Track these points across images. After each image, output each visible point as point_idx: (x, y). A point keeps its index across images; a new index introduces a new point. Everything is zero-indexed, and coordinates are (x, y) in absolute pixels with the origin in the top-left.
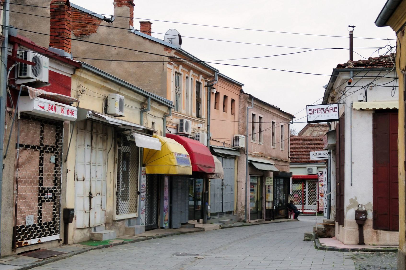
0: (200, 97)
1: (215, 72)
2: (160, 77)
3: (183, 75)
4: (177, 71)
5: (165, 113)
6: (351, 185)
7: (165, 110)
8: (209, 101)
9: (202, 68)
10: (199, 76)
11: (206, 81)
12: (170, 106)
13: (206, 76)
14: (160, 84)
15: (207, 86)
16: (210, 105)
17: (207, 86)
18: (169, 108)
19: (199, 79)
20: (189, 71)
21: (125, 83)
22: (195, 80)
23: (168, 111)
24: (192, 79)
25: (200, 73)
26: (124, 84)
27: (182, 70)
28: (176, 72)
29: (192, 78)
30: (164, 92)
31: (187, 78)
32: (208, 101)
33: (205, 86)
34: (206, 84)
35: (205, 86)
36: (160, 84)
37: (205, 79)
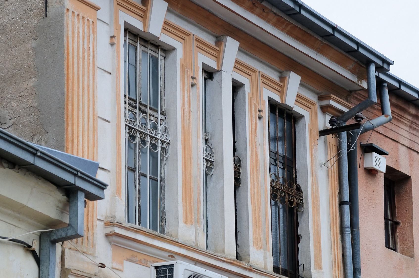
0: (300, 181)
1: (369, 62)
2: (33, 44)
3: (179, 54)
4: (137, 24)
5: (53, 224)
6: (110, 74)
7: (44, 203)
8: (348, 203)
9: (297, 38)
10: (282, 79)
11: (324, 109)
12: (70, 178)
13: (322, 85)
14: (33, 82)
15: (334, 130)
16: (354, 226)
17: (334, 130)
18: (69, 192)
19: (281, 91)
20: (219, 41)
21: (34, 152)
22: (256, 94)
23: (62, 210)
24: (236, 87)
25: (286, 63)
26: (28, 158)
27: (167, 27)
28: (129, 31)
29: (241, 78)
30: (54, 113)
31: (209, 74)
32: (342, 203)
33: (323, 133)
34: (324, 121)
35: (323, 133)
36: (33, 82)
37: (321, 98)
